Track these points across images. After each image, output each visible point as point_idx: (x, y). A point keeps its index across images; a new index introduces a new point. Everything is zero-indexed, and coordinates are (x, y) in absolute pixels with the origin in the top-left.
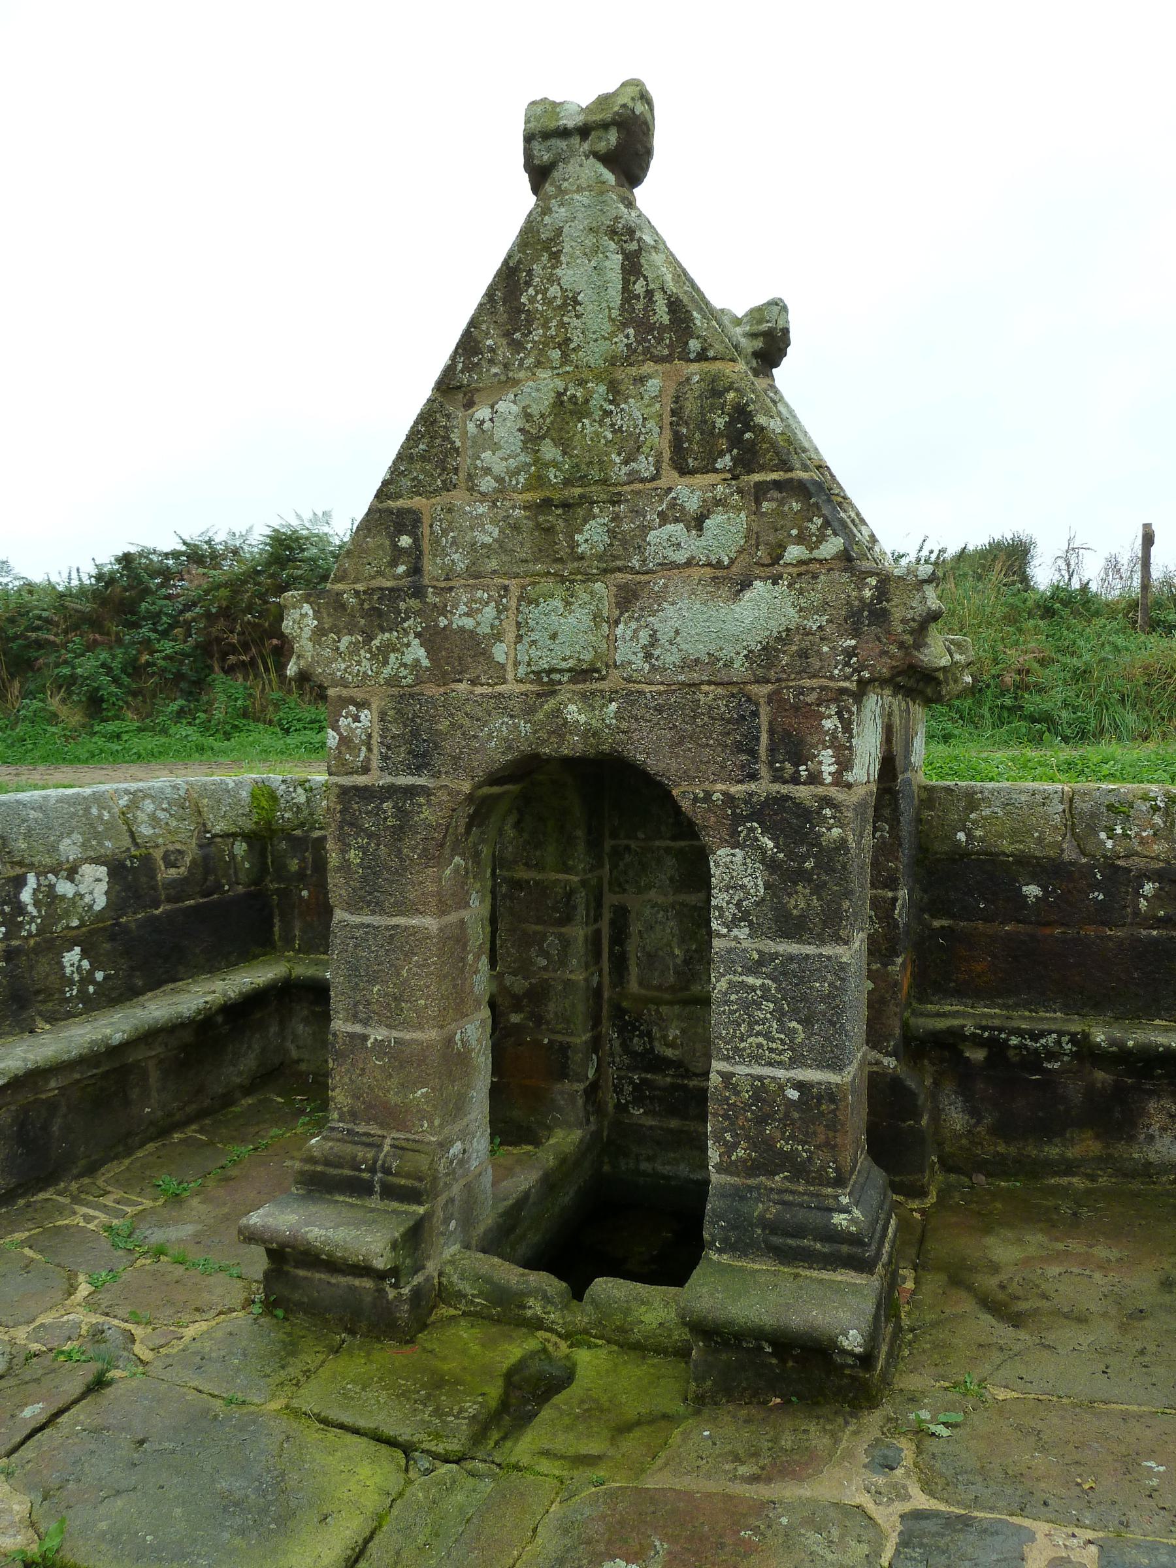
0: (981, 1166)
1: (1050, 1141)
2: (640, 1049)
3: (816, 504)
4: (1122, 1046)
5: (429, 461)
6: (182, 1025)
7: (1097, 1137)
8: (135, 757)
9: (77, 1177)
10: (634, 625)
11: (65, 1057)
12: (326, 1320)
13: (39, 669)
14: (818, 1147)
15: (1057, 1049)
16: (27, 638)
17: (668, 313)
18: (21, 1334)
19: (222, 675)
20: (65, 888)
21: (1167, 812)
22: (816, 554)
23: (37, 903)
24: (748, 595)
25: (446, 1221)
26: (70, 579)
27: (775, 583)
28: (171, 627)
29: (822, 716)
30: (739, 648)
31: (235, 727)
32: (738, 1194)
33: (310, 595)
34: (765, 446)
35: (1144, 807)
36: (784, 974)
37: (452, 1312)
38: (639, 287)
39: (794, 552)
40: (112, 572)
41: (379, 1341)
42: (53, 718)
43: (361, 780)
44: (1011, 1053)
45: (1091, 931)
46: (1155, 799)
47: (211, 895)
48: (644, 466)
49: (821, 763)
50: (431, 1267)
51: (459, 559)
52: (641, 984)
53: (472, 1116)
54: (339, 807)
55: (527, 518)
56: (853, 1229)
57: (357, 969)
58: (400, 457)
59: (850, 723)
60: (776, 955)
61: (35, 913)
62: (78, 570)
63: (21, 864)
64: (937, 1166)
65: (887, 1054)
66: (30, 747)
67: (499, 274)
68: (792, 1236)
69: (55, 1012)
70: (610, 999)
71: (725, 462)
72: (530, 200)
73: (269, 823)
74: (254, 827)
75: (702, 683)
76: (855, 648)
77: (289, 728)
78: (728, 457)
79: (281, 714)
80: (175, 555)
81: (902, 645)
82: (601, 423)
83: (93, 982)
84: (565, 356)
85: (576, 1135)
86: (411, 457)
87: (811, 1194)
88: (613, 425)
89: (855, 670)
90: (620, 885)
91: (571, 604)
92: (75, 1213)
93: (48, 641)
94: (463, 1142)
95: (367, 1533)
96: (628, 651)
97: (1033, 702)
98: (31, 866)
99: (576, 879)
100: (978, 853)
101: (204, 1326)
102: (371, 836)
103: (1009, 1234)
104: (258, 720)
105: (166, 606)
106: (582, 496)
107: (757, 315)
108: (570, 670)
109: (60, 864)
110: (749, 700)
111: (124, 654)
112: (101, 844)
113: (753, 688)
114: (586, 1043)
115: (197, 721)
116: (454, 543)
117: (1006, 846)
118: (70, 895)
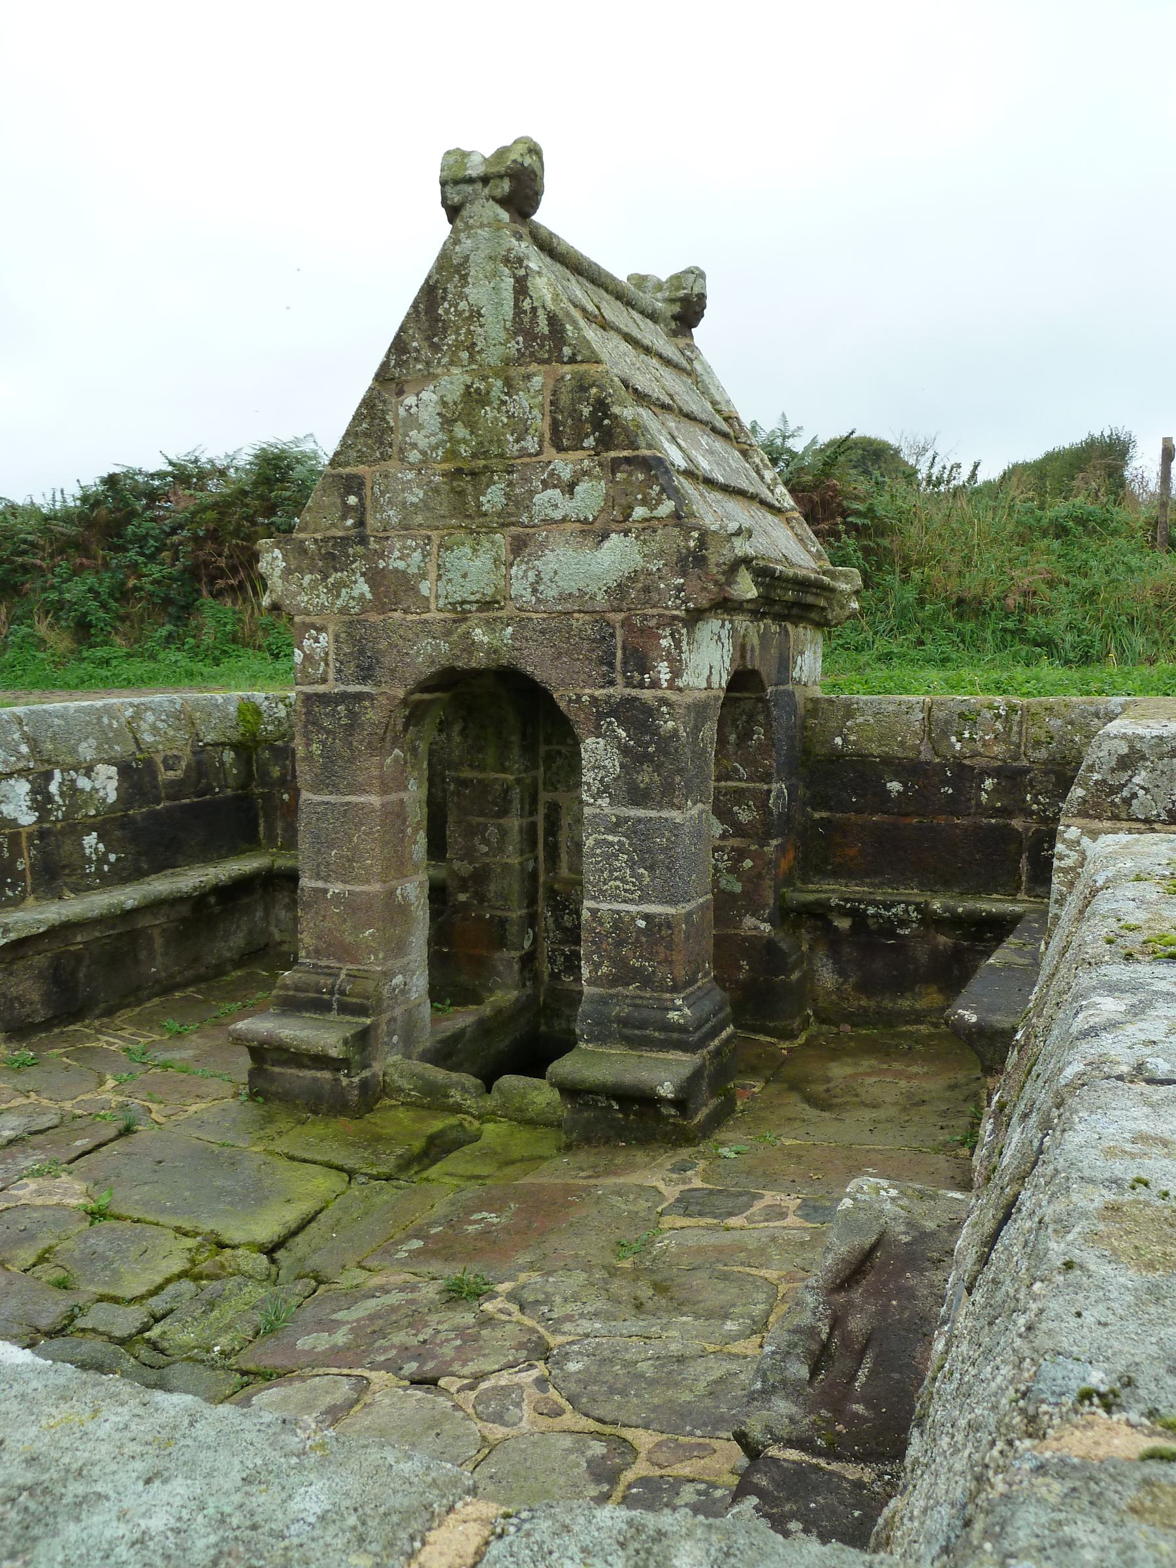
0: (848, 1018)
1: (902, 996)
2: (569, 925)
3: (655, 476)
4: (953, 911)
5: (370, 437)
6: (181, 898)
7: (940, 991)
8: (125, 683)
10: (524, 567)
11: (90, 915)
13: (26, 594)
15: (906, 917)
16: (13, 562)
17: (549, 325)
18: (68, 1105)
19: (211, 599)
20: (83, 783)
21: (1007, 719)
22: (656, 513)
23: (62, 794)
24: (606, 544)
25: (390, 1034)
26: (54, 500)
27: (626, 535)
28: (159, 550)
29: (660, 637)
31: (225, 652)
32: (603, 1001)
33: (280, 542)
34: (618, 430)
35: (989, 714)
36: (635, 833)
37: (394, 1102)
38: (526, 305)
39: (640, 512)
41: (335, 1117)
42: (41, 643)
43: (321, 689)
44: (871, 922)
45: (942, 820)
47: (205, 795)
48: (531, 444)
49: (659, 672)
50: (377, 1067)
51: (393, 515)
52: (570, 869)
53: (412, 957)
54: (304, 710)
55: (445, 483)
56: (682, 1021)
57: (319, 838)
58: (348, 434)
59: (680, 642)
61: (61, 803)
62: (62, 491)
63: (49, 761)
64: (812, 1019)
65: (764, 921)
66: (20, 673)
67: (422, 290)
68: (639, 1028)
69: (78, 884)
70: (545, 882)
71: (590, 442)
72: (444, 228)
73: (254, 735)
74: (240, 738)
75: (574, 612)
76: (683, 584)
77: (278, 654)
78: (592, 438)
79: (271, 639)
80: (161, 475)
81: (716, 583)
83: (108, 862)
84: (471, 356)
86: (356, 434)
87: (655, 999)
88: (507, 412)
89: (683, 602)
90: (552, 784)
92: (99, 1040)
93: (34, 566)
94: (404, 976)
95: (318, 1208)
96: (520, 588)
97: (1036, 625)
99: (512, 777)
100: (851, 755)
101: (203, 1106)
102: (328, 732)
103: (850, 1060)
105: (153, 528)
106: (485, 467)
107: (675, 283)
109: (79, 763)
110: (608, 624)
111: (112, 578)
112: (111, 748)
113: (611, 616)
114: (521, 917)
115: (186, 647)
116: (390, 502)
117: (874, 748)
118: (88, 789)
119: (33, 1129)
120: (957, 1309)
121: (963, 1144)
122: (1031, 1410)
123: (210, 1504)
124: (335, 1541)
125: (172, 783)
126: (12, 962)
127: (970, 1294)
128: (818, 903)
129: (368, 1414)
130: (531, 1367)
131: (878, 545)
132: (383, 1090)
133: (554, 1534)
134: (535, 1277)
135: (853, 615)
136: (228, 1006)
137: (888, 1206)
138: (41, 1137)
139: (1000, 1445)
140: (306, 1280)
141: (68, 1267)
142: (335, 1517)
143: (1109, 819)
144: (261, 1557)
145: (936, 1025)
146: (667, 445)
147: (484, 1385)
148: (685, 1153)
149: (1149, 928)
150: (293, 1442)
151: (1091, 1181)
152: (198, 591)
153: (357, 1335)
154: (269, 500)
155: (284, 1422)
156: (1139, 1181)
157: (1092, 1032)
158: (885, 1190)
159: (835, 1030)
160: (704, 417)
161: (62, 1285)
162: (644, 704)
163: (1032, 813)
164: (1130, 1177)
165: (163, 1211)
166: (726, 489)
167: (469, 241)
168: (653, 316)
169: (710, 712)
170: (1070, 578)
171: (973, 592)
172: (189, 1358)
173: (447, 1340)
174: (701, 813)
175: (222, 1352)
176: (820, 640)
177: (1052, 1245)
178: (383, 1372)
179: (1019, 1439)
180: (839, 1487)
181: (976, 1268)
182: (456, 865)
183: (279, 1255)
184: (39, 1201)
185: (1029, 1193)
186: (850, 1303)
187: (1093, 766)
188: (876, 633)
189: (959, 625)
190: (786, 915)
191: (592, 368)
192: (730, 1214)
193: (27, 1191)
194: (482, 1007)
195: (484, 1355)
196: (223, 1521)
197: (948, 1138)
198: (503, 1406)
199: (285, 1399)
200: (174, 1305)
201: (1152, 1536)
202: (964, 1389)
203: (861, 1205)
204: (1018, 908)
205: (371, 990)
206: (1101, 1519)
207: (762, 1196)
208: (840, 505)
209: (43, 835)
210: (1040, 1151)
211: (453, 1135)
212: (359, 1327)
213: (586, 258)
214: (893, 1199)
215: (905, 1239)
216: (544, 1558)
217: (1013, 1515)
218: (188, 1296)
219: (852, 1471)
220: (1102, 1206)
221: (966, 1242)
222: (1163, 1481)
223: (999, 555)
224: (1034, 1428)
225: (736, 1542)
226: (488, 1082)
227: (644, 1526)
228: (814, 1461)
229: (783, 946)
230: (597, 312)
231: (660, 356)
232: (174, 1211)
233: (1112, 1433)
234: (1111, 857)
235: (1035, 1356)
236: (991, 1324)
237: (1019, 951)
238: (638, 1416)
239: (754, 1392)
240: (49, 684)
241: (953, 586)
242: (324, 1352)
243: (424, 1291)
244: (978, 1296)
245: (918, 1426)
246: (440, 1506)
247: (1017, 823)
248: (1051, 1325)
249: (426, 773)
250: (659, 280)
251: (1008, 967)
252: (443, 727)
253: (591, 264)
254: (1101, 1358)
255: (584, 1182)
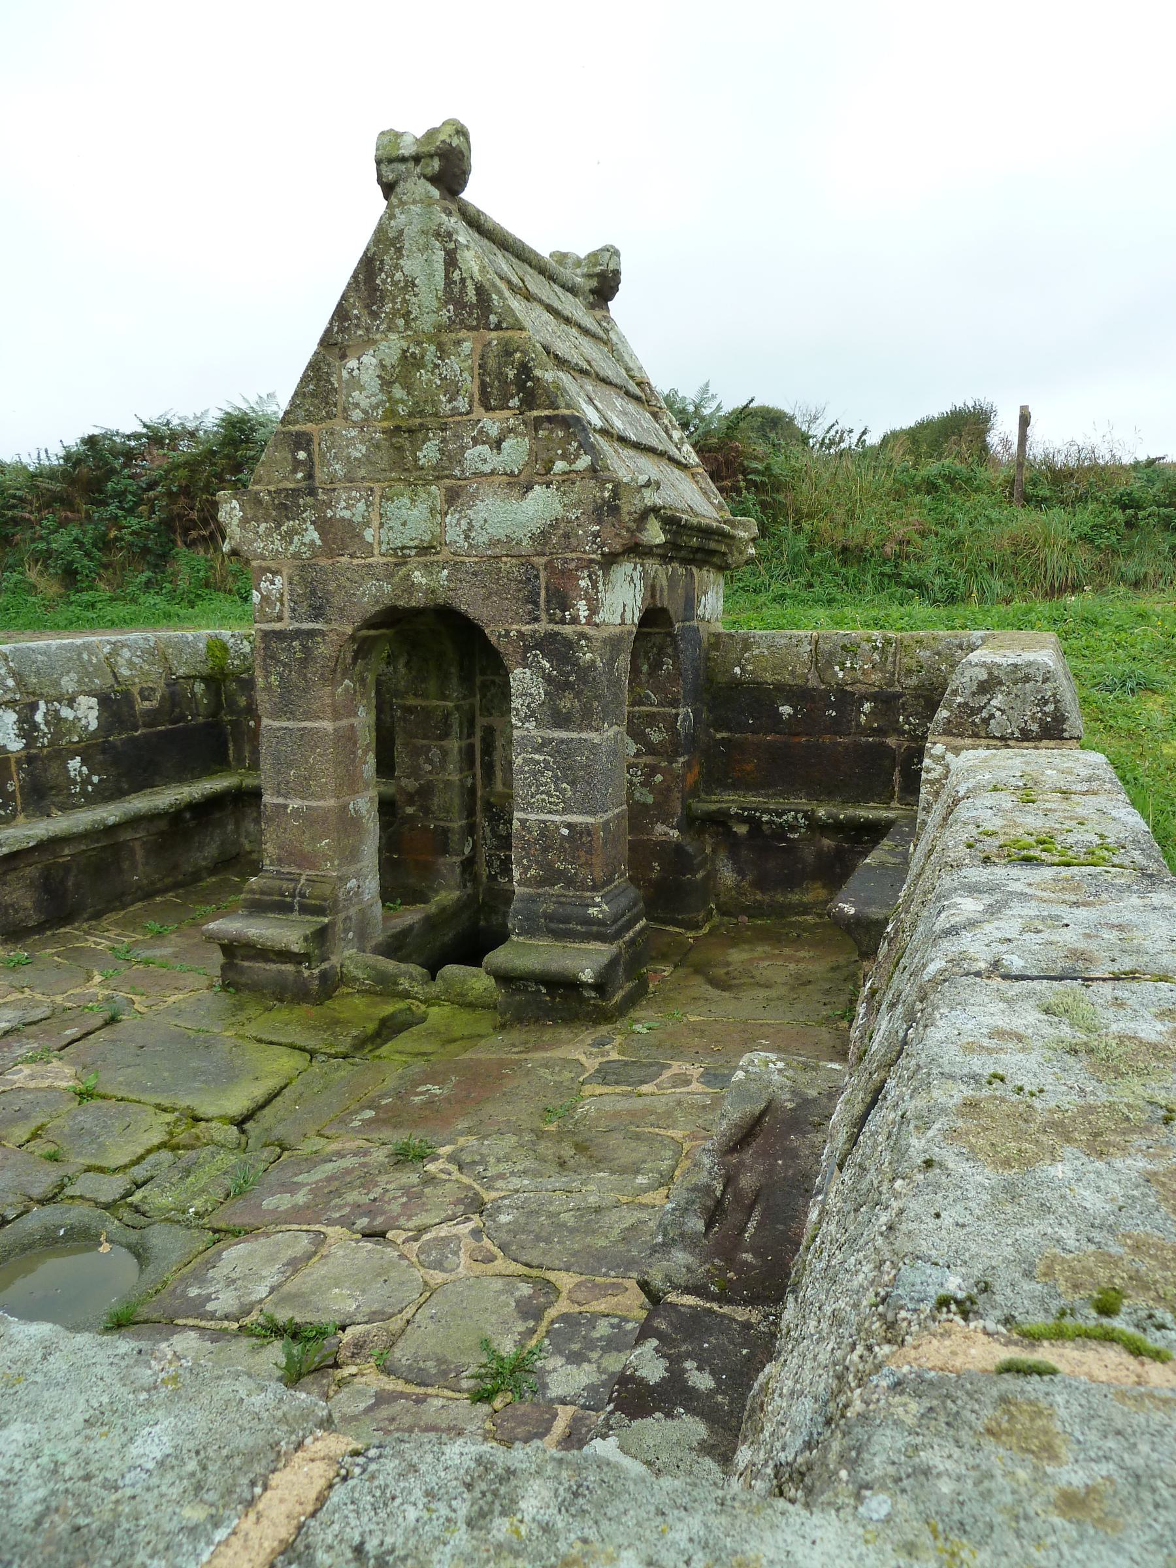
0: (745, 910)
1: (792, 891)
2: (504, 833)
3: (573, 433)
4: (836, 819)
9: (89, 919)
10: (457, 516)
11: (75, 830)
12: (264, 994)
13: (17, 544)
14: (581, 866)
17: (477, 294)
19: (185, 549)
20: (66, 713)
21: (883, 651)
22: (574, 467)
23: (47, 723)
24: (530, 495)
25: (346, 931)
26: (39, 460)
28: (137, 504)
29: (579, 578)
30: (526, 531)
31: (198, 596)
32: (532, 899)
35: (867, 647)
36: (558, 752)
37: (350, 990)
39: (560, 466)
40: (78, 453)
42: (33, 589)
43: (277, 626)
44: (765, 827)
46: (875, 641)
48: (462, 404)
50: (335, 960)
51: (339, 468)
52: (504, 785)
54: (263, 646)
58: (296, 394)
59: (597, 582)
60: (553, 739)
62: (46, 451)
63: (34, 694)
65: (673, 828)
66: (13, 615)
69: (64, 803)
70: (482, 796)
71: (515, 402)
73: (222, 669)
76: (599, 531)
80: (136, 436)
81: (628, 530)
82: (433, 373)
83: (91, 783)
85: (456, 894)
86: (304, 395)
88: (440, 374)
90: (488, 710)
91: (415, 501)
93: (23, 519)
96: (454, 535)
97: (910, 569)
98: (41, 696)
100: (748, 683)
101: (181, 997)
102: (285, 665)
103: (746, 947)
104: (219, 590)
105: (131, 485)
106: (421, 425)
108: (416, 547)
109: (62, 695)
110: (533, 567)
116: (336, 457)
117: (768, 677)
118: (71, 718)
119: (27, 1021)
120: (829, 1182)
121: (842, 1017)
122: (890, 1317)
123: (46, 1452)
124: (171, 1490)
125: (148, 713)
126: (5, 873)
127: (841, 1169)
128: (719, 812)
129: (325, 1264)
130: (468, 1219)
131: (774, 499)
132: (341, 980)
133: (399, 1475)
134: (472, 1141)
135: (750, 561)
136: (204, 908)
137: (775, 1077)
138: (34, 1028)
139: (860, 1349)
140: (272, 1148)
141: (59, 1142)
142: (174, 1462)
143: (970, 737)
144: (89, 1513)
145: (820, 916)
146: (584, 406)
147: (426, 1237)
148: (604, 1030)
149: (1005, 833)
150: (145, 1375)
151: (951, 1077)
152: (174, 542)
153: (316, 1196)
154: (235, 458)
155: (140, 1352)
156: (995, 1076)
157: (952, 931)
158: (773, 1063)
159: (735, 921)
160: (618, 381)
161: (53, 1158)
162: (565, 639)
163: (904, 732)
164: (987, 1072)
165: (145, 1090)
166: (637, 446)
167: (403, 216)
168: (572, 290)
169: (624, 645)
170: (940, 530)
171: (856, 541)
172: (167, 1219)
173: (394, 1198)
174: (616, 734)
175: (196, 1213)
176: (722, 582)
177: (914, 1141)
178: (338, 1227)
179: (879, 1345)
180: (730, 1328)
181: (847, 1146)
182: (404, 782)
183: (248, 1126)
184: (32, 1085)
185: (894, 1082)
186: (741, 1163)
187: (957, 690)
188: (772, 577)
189: (844, 570)
190: (693, 823)
191: (516, 335)
192: (643, 1082)
193: (21, 1076)
194: (428, 906)
195: (426, 1211)
196: (55, 1472)
197: (830, 1013)
198: (443, 1255)
199: (251, 1254)
200: (155, 1173)
201: (1009, 1462)
202: (831, 1272)
203: (752, 1076)
204: (891, 815)
205: (328, 892)
206: (958, 1444)
207: (670, 1066)
208: (741, 464)
209: (30, 759)
210: (905, 1042)
211: (402, 1018)
212: (317, 1188)
213: (511, 235)
214: (780, 1071)
215: (790, 1105)
216: (385, 1505)
217: (869, 1439)
218: (166, 1164)
219: (741, 1314)
220: (960, 1102)
221: (840, 1115)
222: (1020, 1399)
223: (878, 508)
224: (893, 1334)
225: (586, 1479)
226: (433, 969)
227: (493, 1463)
228: (708, 1305)
229: (690, 850)
230: (521, 285)
231: (579, 326)
232: (154, 1090)
233: (969, 1342)
234: (972, 770)
235: (895, 1258)
236: (856, 1210)
237: (891, 852)
238: (561, 1260)
239: (656, 1245)
240: (40, 625)
241: (839, 536)
242: (286, 1211)
243: (375, 1155)
244: (847, 1175)
245: (793, 1291)
246: (288, 1443)
247: (891, 741)
248: (913, 1226)
249: (374, 702)
250: (578, 257)
251: (882, 865)
252: (390, 660)
253: (516, 240)
254: (959, 1262)
255: (516, 1057)
